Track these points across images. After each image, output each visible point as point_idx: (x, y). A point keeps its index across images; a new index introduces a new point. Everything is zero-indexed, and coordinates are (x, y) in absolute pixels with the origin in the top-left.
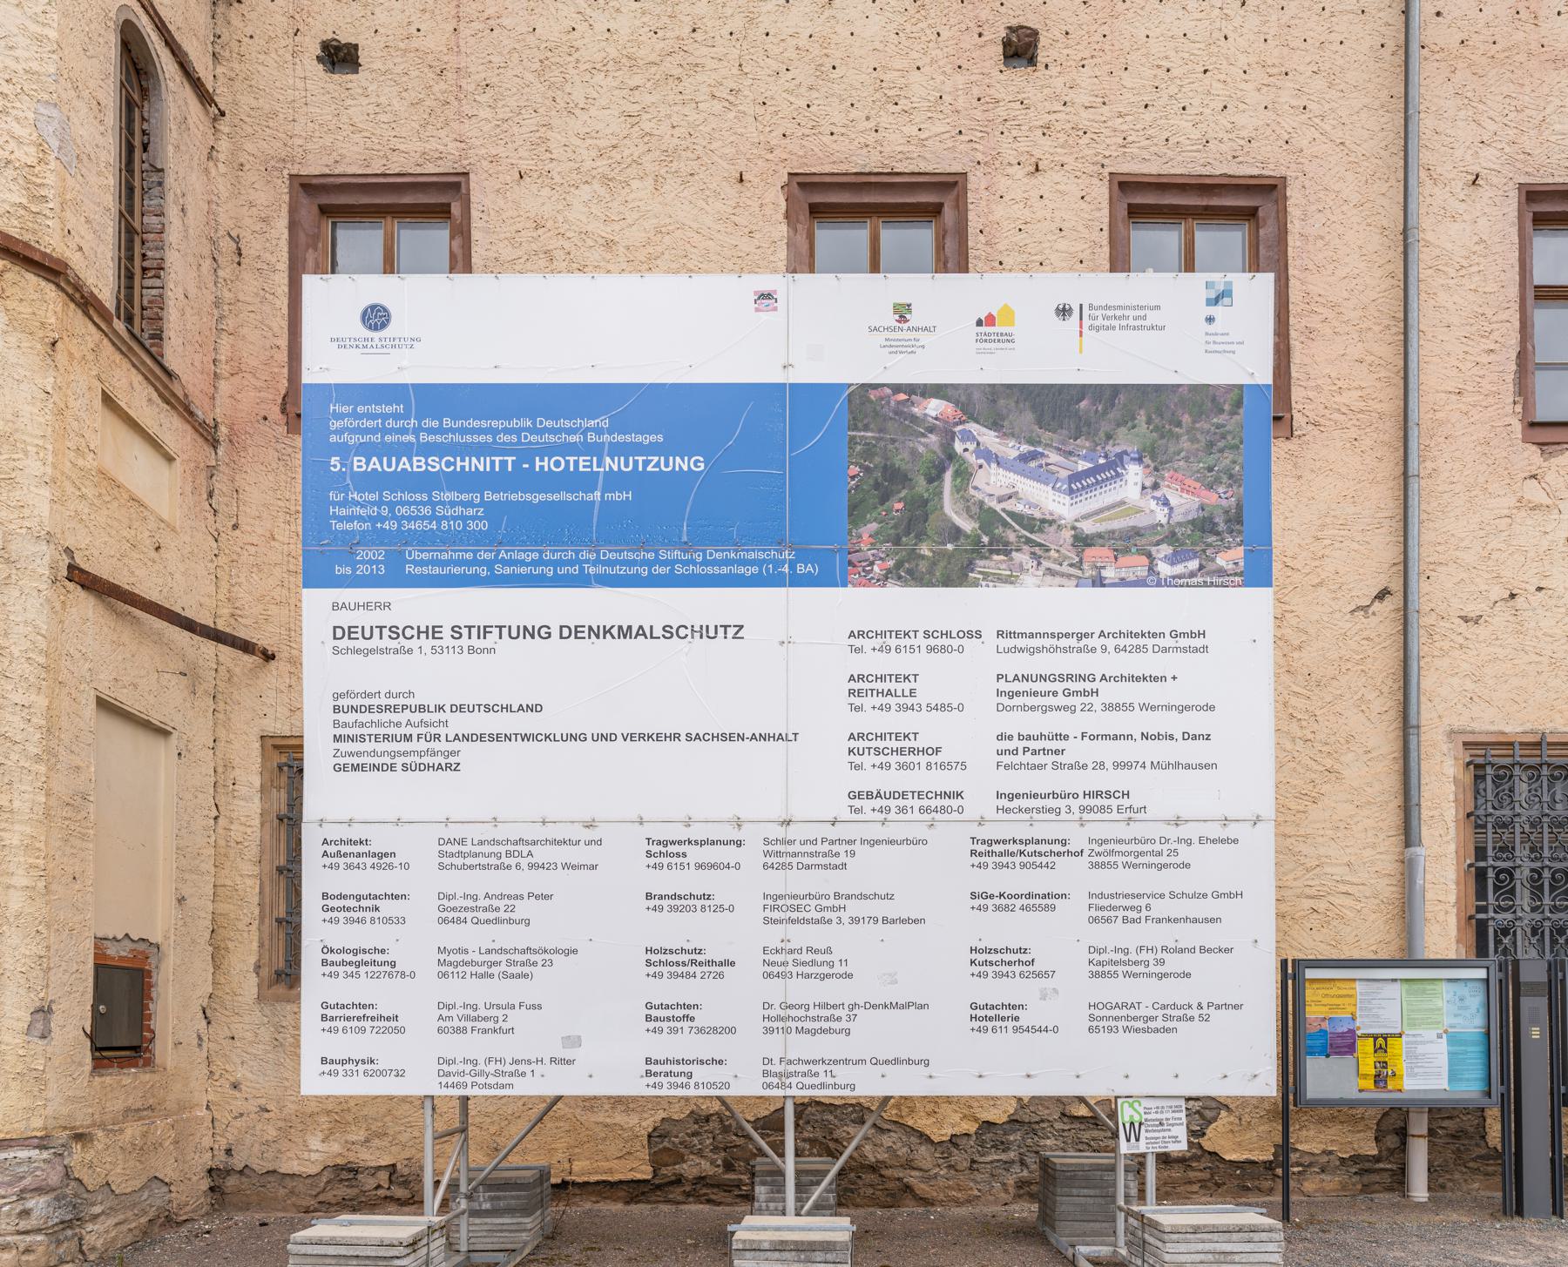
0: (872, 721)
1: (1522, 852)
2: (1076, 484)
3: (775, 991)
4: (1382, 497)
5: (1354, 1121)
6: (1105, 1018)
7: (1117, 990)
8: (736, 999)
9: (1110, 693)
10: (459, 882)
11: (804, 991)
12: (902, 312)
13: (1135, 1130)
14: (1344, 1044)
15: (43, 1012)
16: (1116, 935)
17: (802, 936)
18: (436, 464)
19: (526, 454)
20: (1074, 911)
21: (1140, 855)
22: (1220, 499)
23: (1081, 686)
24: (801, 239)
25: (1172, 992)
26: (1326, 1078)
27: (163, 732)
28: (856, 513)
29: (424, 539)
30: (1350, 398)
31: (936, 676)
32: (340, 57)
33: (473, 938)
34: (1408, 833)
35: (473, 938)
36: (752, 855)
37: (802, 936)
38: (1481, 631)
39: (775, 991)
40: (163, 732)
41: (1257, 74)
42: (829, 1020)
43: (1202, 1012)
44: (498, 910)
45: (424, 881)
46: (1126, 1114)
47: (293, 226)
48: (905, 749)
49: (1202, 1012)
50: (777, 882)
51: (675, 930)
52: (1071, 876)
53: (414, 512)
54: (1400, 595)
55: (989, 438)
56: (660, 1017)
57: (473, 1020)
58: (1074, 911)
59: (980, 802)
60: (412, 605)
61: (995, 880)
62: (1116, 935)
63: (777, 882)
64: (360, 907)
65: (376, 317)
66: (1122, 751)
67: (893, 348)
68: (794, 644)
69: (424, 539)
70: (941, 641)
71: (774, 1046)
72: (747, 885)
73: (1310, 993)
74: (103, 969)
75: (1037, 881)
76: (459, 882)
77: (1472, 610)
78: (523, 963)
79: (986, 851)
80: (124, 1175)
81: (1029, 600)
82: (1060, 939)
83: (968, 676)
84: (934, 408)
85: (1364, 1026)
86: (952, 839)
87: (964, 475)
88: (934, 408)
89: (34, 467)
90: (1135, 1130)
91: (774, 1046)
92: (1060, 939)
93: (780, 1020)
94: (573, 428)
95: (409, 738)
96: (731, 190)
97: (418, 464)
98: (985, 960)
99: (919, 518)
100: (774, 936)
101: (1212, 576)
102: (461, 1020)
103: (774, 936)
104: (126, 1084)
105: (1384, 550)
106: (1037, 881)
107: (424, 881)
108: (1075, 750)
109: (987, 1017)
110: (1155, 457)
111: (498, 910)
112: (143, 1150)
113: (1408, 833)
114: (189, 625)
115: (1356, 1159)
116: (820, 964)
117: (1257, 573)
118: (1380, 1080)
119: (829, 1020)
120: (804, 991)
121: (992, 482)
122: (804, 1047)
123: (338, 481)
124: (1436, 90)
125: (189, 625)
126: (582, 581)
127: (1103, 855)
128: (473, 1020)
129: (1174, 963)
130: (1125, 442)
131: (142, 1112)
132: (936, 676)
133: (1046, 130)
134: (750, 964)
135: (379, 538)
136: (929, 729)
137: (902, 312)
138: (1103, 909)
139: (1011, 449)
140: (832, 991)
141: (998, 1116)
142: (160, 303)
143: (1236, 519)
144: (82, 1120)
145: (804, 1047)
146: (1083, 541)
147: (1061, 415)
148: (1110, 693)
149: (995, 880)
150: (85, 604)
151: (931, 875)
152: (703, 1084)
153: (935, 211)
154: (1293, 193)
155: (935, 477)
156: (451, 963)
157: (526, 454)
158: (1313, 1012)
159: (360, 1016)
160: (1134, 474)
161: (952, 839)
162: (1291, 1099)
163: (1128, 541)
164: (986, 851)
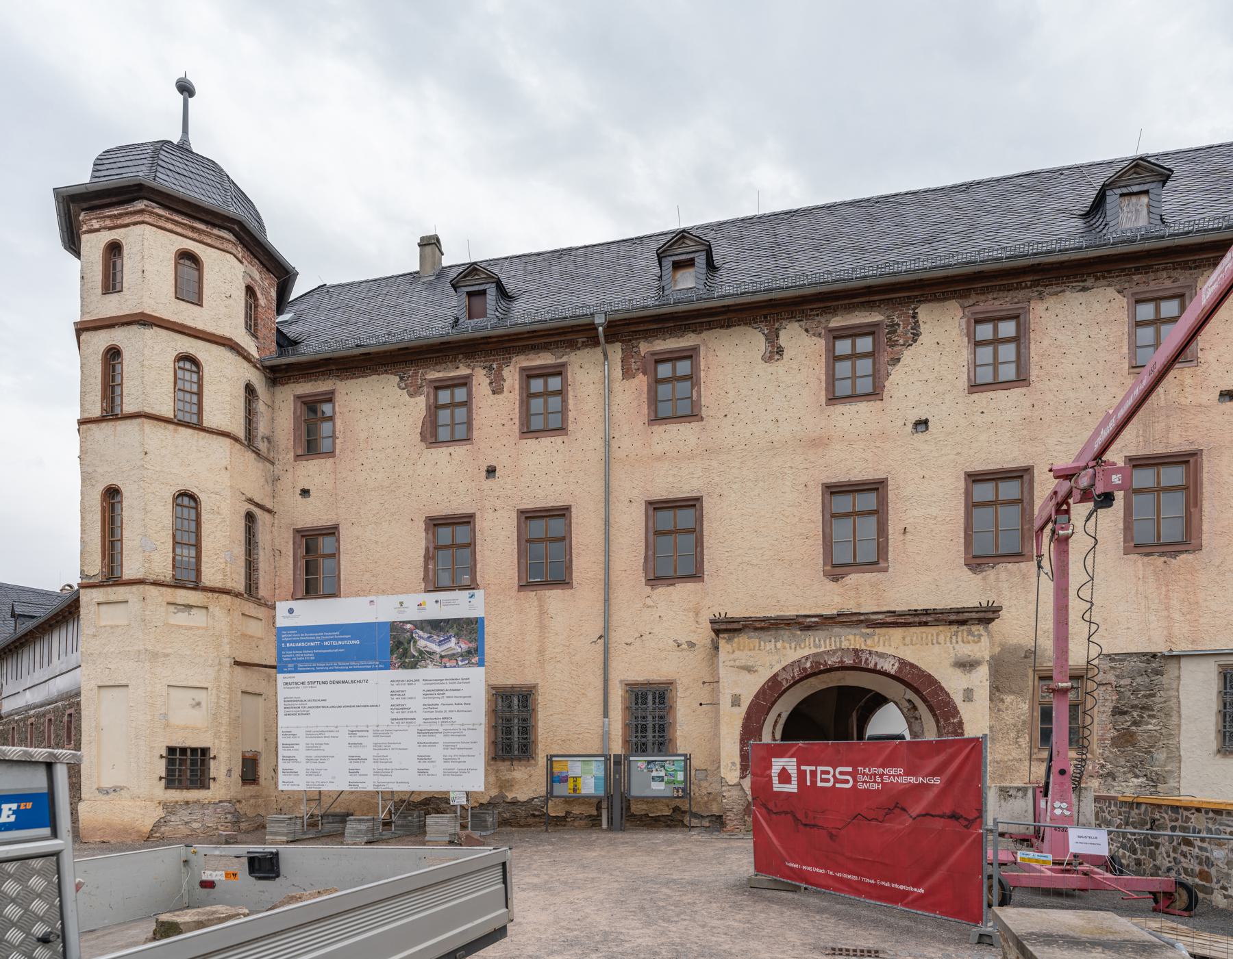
0: (396, 702)
1: (650, 718)
2: (440, 643)
3: (375, 766)
4: (600, 606)
5: (590, 804)
6: (448, 772)
7: (450, 765)
8: (367, 768)
9: (448, 693)
10: (310, 741)
11: (382, 766)
12: (401, 604)
13: (454, 799)
14: (564, 780)
15: (229, 771)
16: (449, 752)
17: (382, 753)
18: (304, 644)
19: (322, 641)
20: (440, 747)
21: (455, 733)
22: (473, 645)
23: (441, 692)
24: (430, 536)
25: (462, 766)
26: (560, 790)
27: (260, 695)
28: (392, 652)
29: (302, 662)
30: (590, 575)
31: (410, 690)
32: (305, 493)
33: (313, 754)
34: (606, 714)
35: (313, 754)
36: (370, 734)
37: (382, 753)
38: (631, 648)
39: (375, 766)
40: (260, 695)
41: (562, 473)
42: (387, 773)
43: (468, 771)
44: (316, 747)
45: (302, 741)
46: (452, 795)
47: (294, 543)
48: (403, 708)
49: (468, 771)
50: (376, 740)
51: (354, 752)
52: (439, 738)
53: (299, 655)
54: (605, 637)
55: (421, 633)
56: (353, 772)
57: (315, 773)
58: (440, 747)
59: (419, 721)
60: (300, 677)
61: (423, 739)
62: (449, 752)
63: (376, 740)
64: (288, 747)
65: (291, 611)
66: (451, 708)
67: (400, 612)
68: (378, 684)
69: (302, 662)
70: (411, 682)
71: (376, 779)
72: (369, 741)
73: (555, 765)
74: (245, 760)
75: (432, 739)
76: (310, 741)
77: (629, 641)
78: (323, 759)
79: (421, 732)
80: (251, 813)
81: (430, 672)
82: (437, 753)
83: (416, 691)
84: (409, 626)
85: (571, 774)
86: (413, 730)
87: (415, 642)
88: (409, 626)
89: (226, 641)
90: (454, 799)
91: (376, 779)
92: (437, 753)
93: (377, 773)
94: (330, 635)
95: (299, 708)
96: (410, 523)
97: (300, 644)
98: (421, 758)
99: (405, 653)
100: (375, 753)
101: (470, 664)
102: (311, 773)
103: (375, 753)
104: (251, 789)
105: (600, 623)
106: (432, 739)
107: (302, 741)
108: (440, 708)
109: (422, 772)
110: (458, 636)
111: (316, 747)
112: (255, 806)
113: (606, 714)
114: (266, 666)
115: (590, 816)
116: (385, 760)
117: (481, 663)
118: (575, 790)
119: (387, 773)
120: (382, 766)
121: (422, 643)
122: (382, 779)
123: (284, 649)
124: (618, 473)
125: (266, 666)
126: (334, 670)
127: (446, 733)
128: (315, 773)
129: (462, 759)
130: (451, 633)
131: (256, 797)
132: (410, 690)
133: (498, 497)
134: (370, 760)
135: (293, 662)
136: (408, 703)
137: (401, 604)
138: (447, 746)
139: (426, 635)
140: (388, 766)
141: (484, 801)
142: (257, 579)
143: (476, 650)
144: (239, 797)
145: (382, 779)
146: (442, 657)
147: (437, 626)
148: (448, 693)
149: (423, 739)
150: (238, 669)
151: (408, 737)
152: (361, 787)
153: (469, 523)
154: (573, 510)
155: (409, 643)
156: (309, 760)
157: (322, 641)
158: (555, 770)
159: (289, 772)
160: (453, 640)
161: (413, 730)
162: (550, 795)
163: (452, 657)
164: (421, 732)
